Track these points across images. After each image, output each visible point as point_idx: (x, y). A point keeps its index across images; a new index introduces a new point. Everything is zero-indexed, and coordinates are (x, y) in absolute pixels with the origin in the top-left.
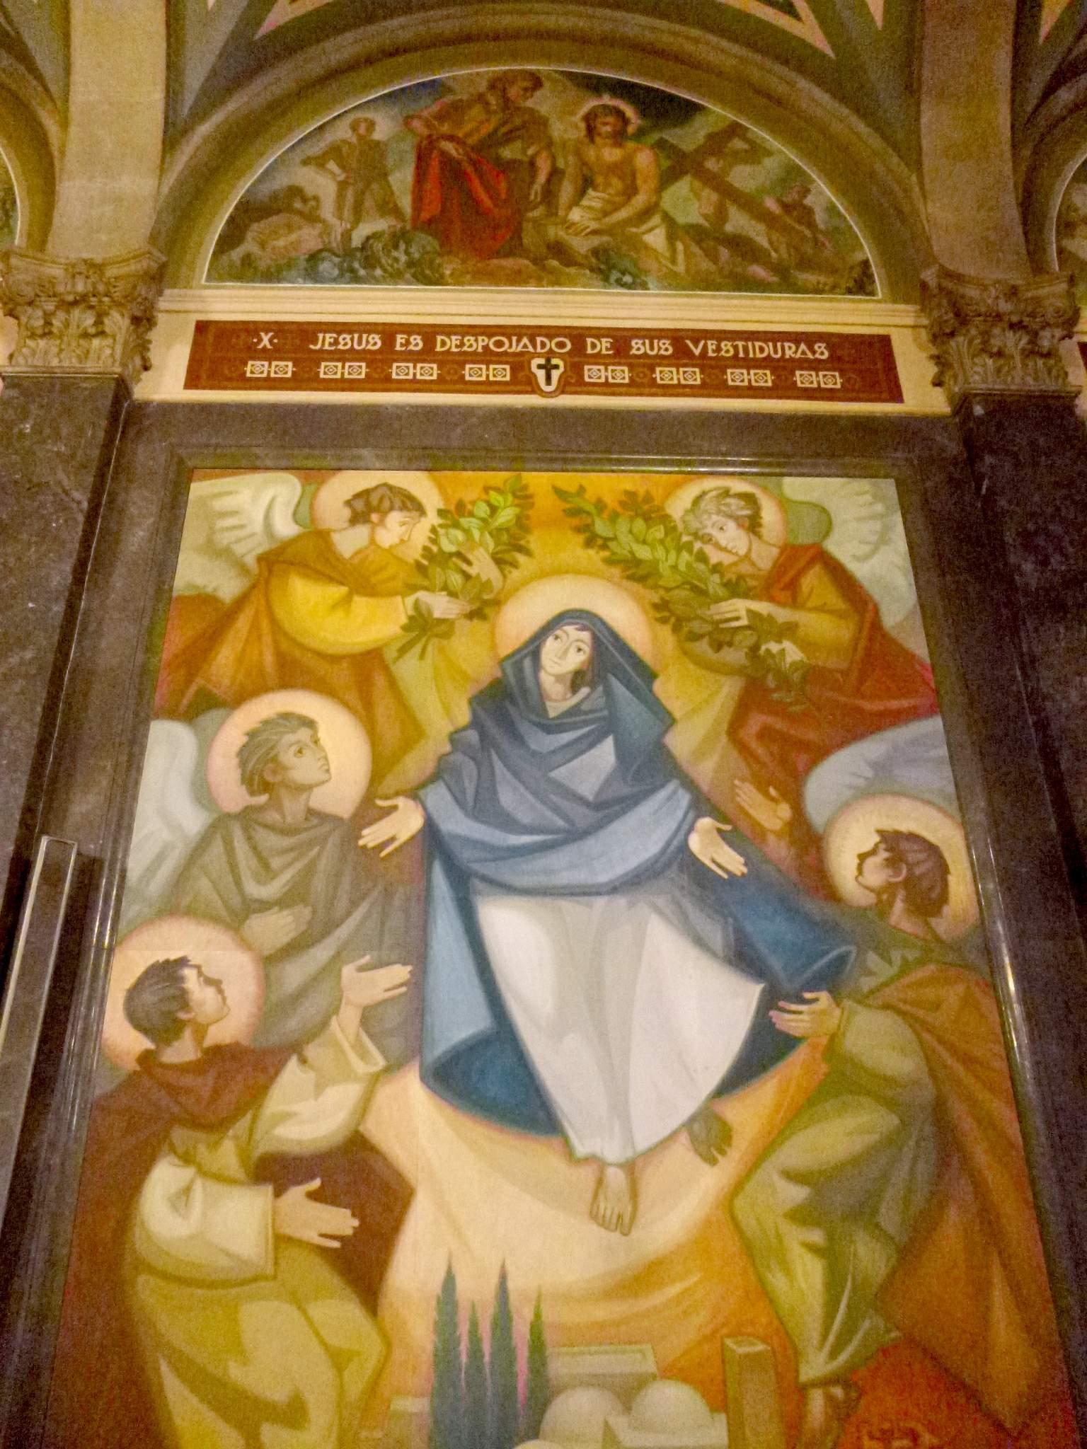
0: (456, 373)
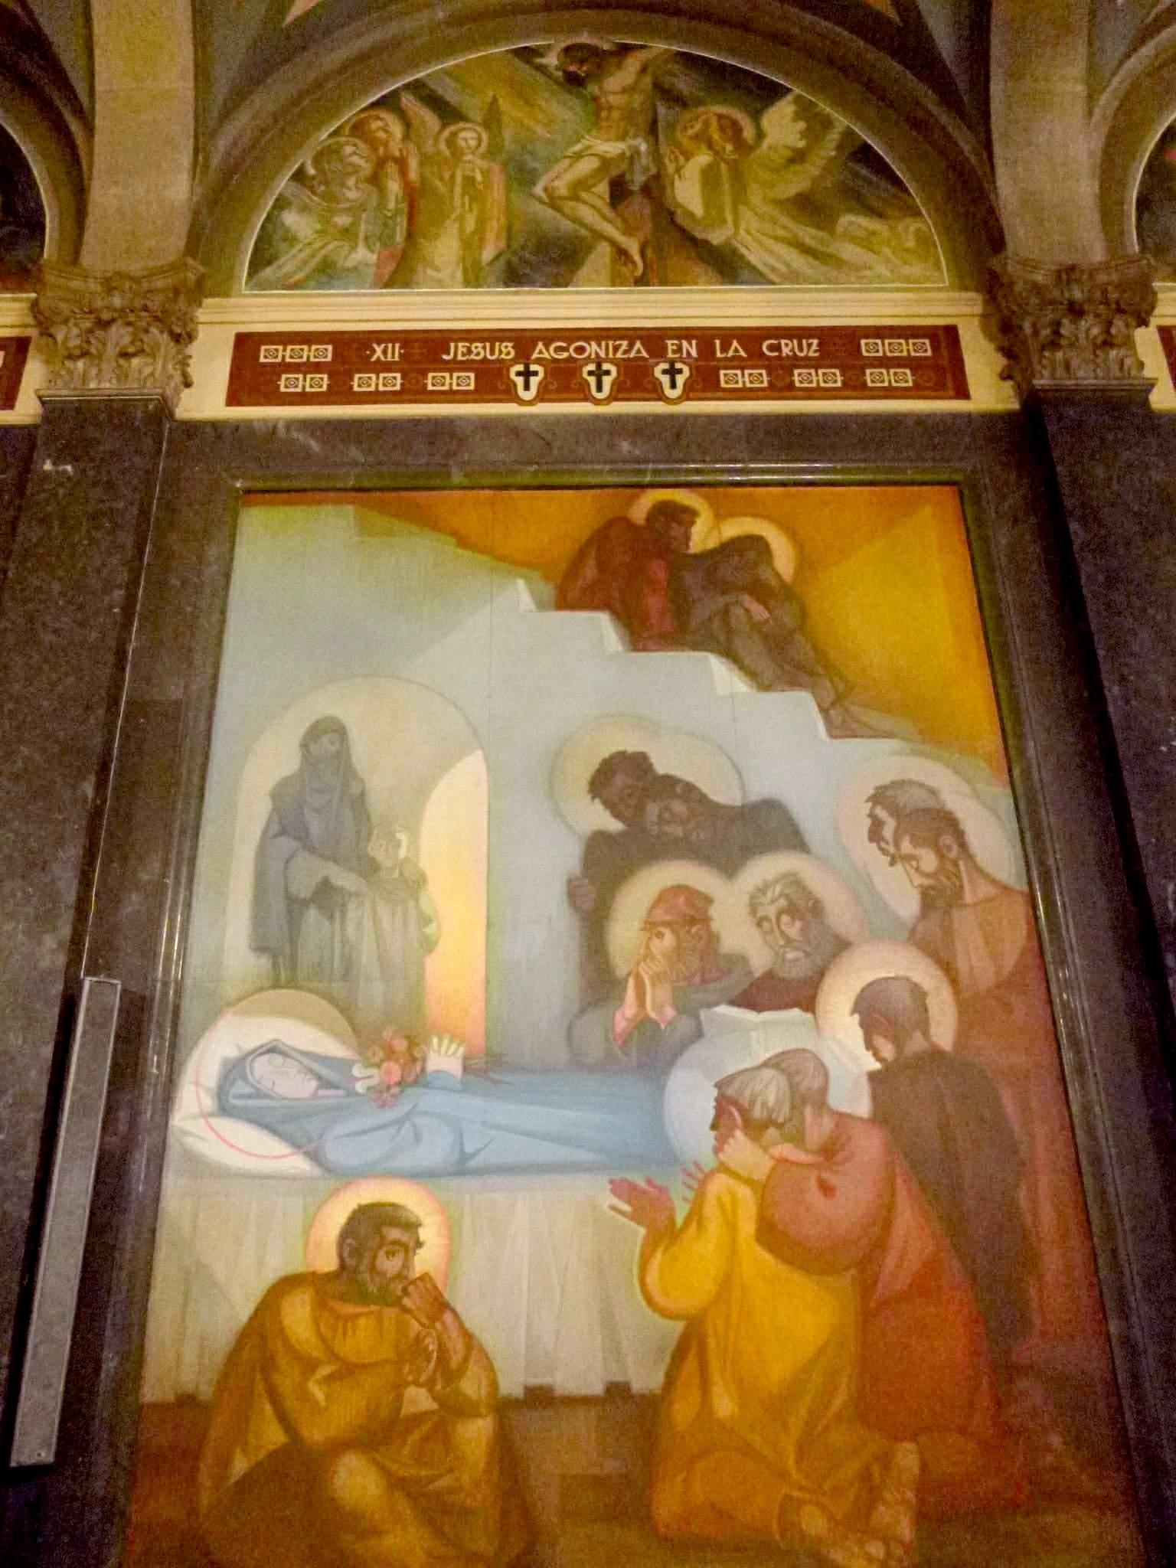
0: (418, 382)
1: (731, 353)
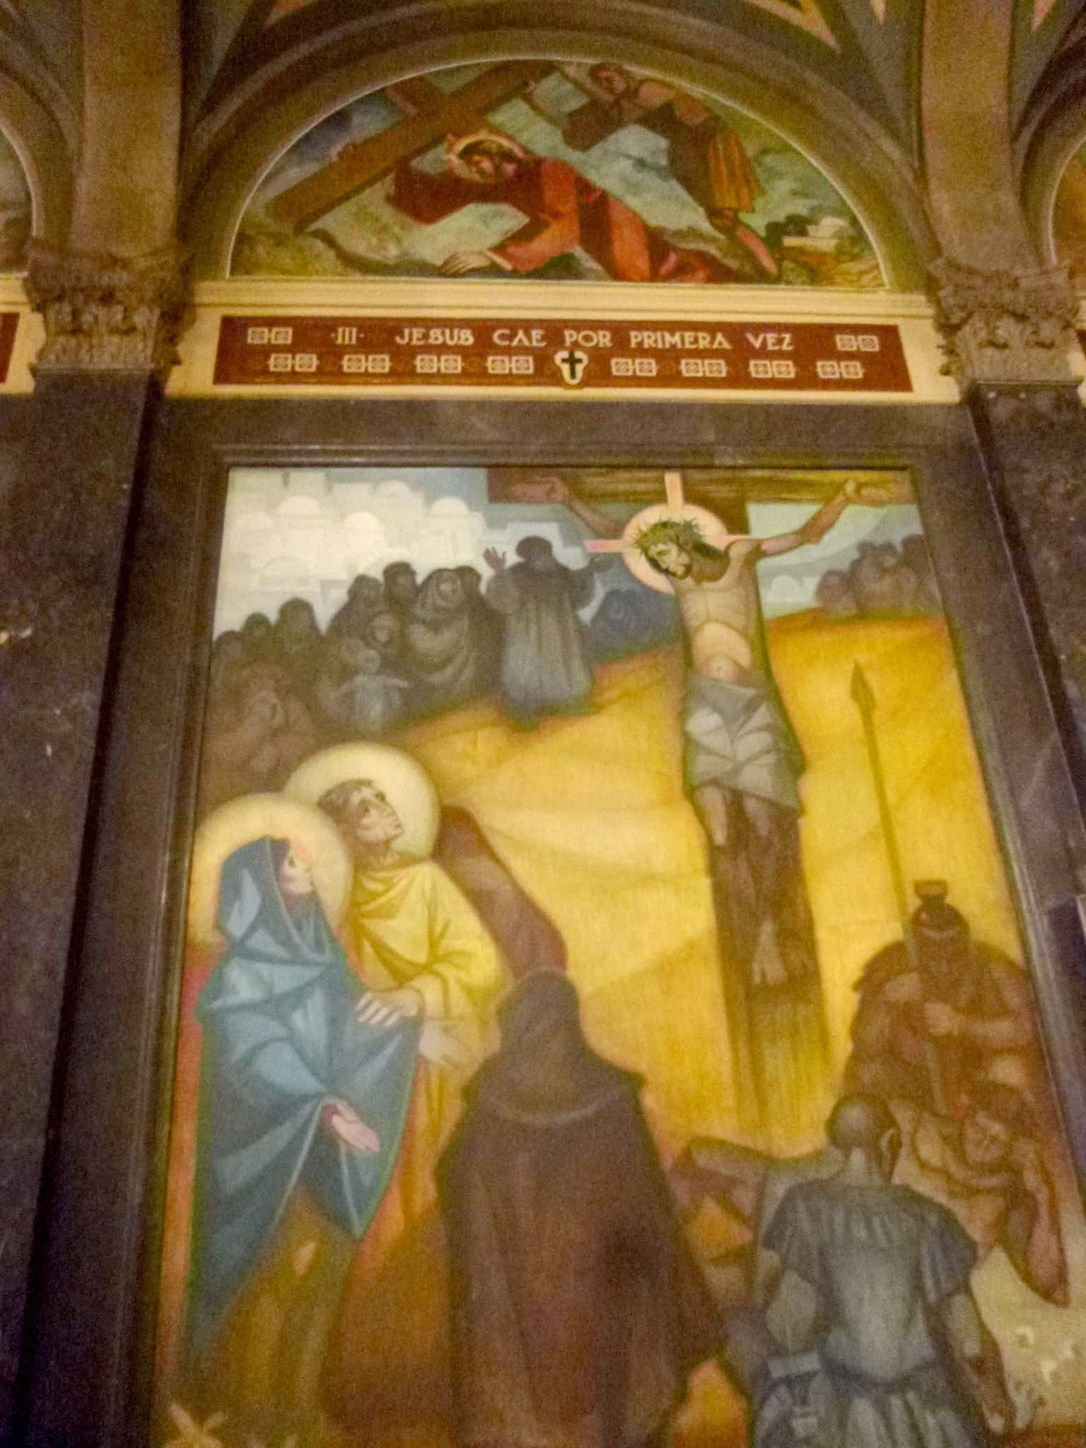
1: (515, 343)
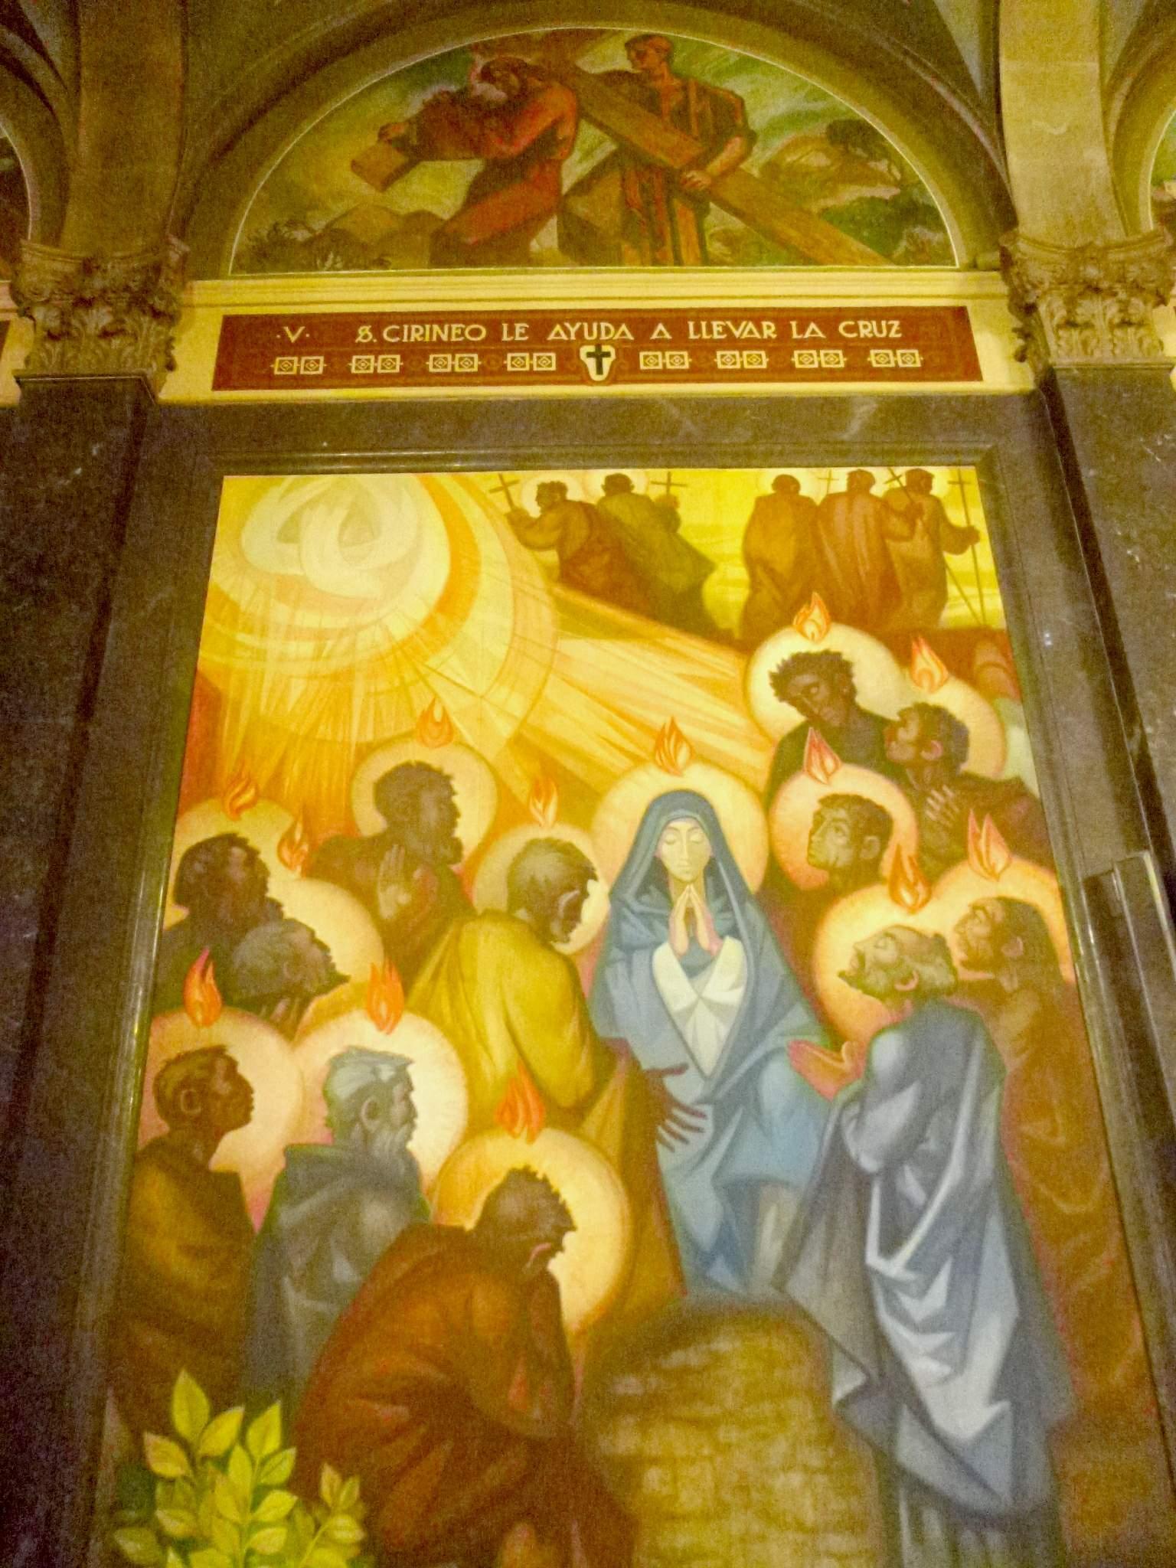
0: (708, 360)
1: (807, 335)
